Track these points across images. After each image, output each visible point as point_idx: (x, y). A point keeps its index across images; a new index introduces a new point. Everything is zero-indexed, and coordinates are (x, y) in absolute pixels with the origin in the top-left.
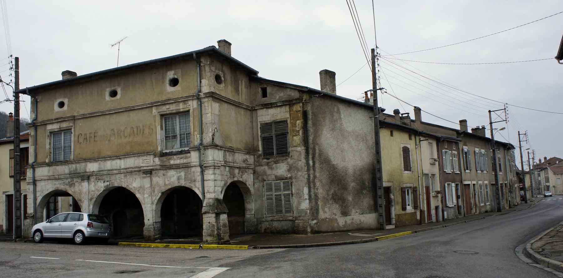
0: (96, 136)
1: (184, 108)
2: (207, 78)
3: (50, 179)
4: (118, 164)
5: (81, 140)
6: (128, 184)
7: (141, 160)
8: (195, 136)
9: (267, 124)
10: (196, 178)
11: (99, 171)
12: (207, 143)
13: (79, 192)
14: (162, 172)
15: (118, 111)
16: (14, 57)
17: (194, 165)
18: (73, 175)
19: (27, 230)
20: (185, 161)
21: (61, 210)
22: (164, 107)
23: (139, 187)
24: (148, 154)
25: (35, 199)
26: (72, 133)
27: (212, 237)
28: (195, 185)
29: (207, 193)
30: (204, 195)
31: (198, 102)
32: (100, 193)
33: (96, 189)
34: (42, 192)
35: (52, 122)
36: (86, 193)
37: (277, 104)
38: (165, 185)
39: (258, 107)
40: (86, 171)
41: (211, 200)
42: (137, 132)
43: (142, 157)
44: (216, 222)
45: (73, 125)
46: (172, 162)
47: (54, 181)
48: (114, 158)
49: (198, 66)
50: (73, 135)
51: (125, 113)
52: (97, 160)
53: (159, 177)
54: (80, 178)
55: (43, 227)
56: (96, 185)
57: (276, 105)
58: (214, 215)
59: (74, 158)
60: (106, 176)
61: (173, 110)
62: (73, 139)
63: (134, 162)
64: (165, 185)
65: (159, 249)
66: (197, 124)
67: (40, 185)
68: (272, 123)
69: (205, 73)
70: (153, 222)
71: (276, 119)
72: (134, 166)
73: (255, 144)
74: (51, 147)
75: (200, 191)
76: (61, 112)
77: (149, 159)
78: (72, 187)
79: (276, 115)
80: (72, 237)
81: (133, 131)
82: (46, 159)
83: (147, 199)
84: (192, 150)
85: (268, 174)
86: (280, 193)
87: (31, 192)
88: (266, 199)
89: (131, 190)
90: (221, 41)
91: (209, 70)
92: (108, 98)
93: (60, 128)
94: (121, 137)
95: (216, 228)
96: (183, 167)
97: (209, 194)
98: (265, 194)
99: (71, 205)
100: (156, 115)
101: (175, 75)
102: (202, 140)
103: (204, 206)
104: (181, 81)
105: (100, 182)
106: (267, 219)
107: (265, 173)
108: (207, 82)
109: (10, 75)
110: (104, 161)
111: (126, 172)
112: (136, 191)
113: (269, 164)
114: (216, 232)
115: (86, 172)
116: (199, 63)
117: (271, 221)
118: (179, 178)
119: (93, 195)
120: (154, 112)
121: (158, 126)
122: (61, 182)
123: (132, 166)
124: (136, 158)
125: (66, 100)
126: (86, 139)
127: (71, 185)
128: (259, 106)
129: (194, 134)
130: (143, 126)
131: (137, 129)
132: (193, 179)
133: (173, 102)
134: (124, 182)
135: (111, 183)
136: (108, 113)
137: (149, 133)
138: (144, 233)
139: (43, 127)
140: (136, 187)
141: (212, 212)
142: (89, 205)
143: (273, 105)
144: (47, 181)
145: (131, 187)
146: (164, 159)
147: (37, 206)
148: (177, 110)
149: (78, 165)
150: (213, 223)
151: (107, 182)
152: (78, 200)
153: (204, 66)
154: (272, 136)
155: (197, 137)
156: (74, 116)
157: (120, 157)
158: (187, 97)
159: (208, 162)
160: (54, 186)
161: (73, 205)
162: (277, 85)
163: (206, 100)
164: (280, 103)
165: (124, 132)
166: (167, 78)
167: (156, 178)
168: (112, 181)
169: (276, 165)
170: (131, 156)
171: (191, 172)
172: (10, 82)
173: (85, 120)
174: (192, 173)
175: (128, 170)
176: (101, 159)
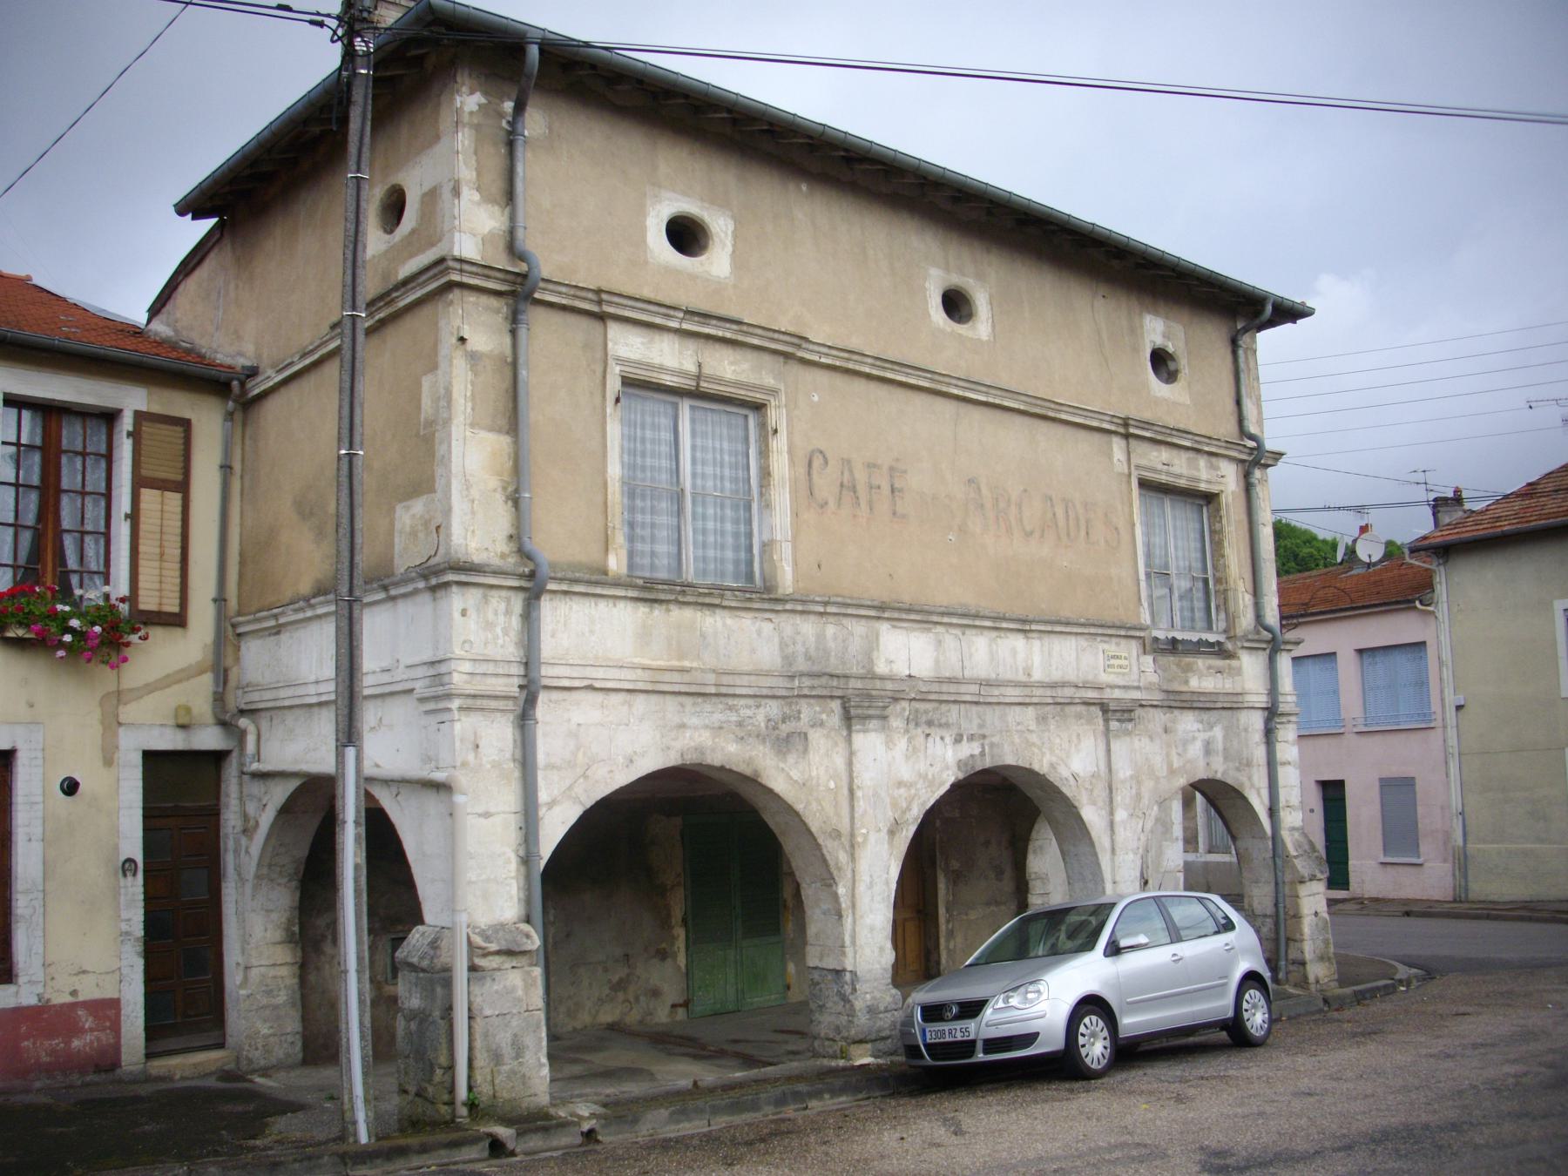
4: (1021, 656)
5: (825, 482)
6: (1054, 759)
13: (832, 785)
14: (1158, 718)
18: (807, 682)
19: (507, 1051)
21: (38, 904)
22: (1155, 454)
28: (1250, 778)
33: (920, 775)
34: (585, 776)
35: (658, 320)
36: (876, 794)
40: (874, 673)
43: (1101, 641)
45: (783, 389)
48: (1012, 626)
53: (1151, 738)
56: (921, 755)
61: (1180, 476)
62: (780, 464)
64: (1172, 772)
72: (1078, 676)
75: (1262, 802)
77: (1126, 658)
81: (1054, 514)
87: (496, 765)
93: (698, 377)
99: (128, 866)
104: (1187, 371)
105: (938, 739)
110: (957, 631)
111: (1050, 700)
112: (1084, 792)
119: (904, 805)
122: (718, 717)
127: (788, 742)
134: (1040, 749)
144: (621, 697)
145: (1064, 772)
149: (830, 630)
152: (824, 833)
165: (1019, 506)
171: (1238, 728)
173: (839, 380)
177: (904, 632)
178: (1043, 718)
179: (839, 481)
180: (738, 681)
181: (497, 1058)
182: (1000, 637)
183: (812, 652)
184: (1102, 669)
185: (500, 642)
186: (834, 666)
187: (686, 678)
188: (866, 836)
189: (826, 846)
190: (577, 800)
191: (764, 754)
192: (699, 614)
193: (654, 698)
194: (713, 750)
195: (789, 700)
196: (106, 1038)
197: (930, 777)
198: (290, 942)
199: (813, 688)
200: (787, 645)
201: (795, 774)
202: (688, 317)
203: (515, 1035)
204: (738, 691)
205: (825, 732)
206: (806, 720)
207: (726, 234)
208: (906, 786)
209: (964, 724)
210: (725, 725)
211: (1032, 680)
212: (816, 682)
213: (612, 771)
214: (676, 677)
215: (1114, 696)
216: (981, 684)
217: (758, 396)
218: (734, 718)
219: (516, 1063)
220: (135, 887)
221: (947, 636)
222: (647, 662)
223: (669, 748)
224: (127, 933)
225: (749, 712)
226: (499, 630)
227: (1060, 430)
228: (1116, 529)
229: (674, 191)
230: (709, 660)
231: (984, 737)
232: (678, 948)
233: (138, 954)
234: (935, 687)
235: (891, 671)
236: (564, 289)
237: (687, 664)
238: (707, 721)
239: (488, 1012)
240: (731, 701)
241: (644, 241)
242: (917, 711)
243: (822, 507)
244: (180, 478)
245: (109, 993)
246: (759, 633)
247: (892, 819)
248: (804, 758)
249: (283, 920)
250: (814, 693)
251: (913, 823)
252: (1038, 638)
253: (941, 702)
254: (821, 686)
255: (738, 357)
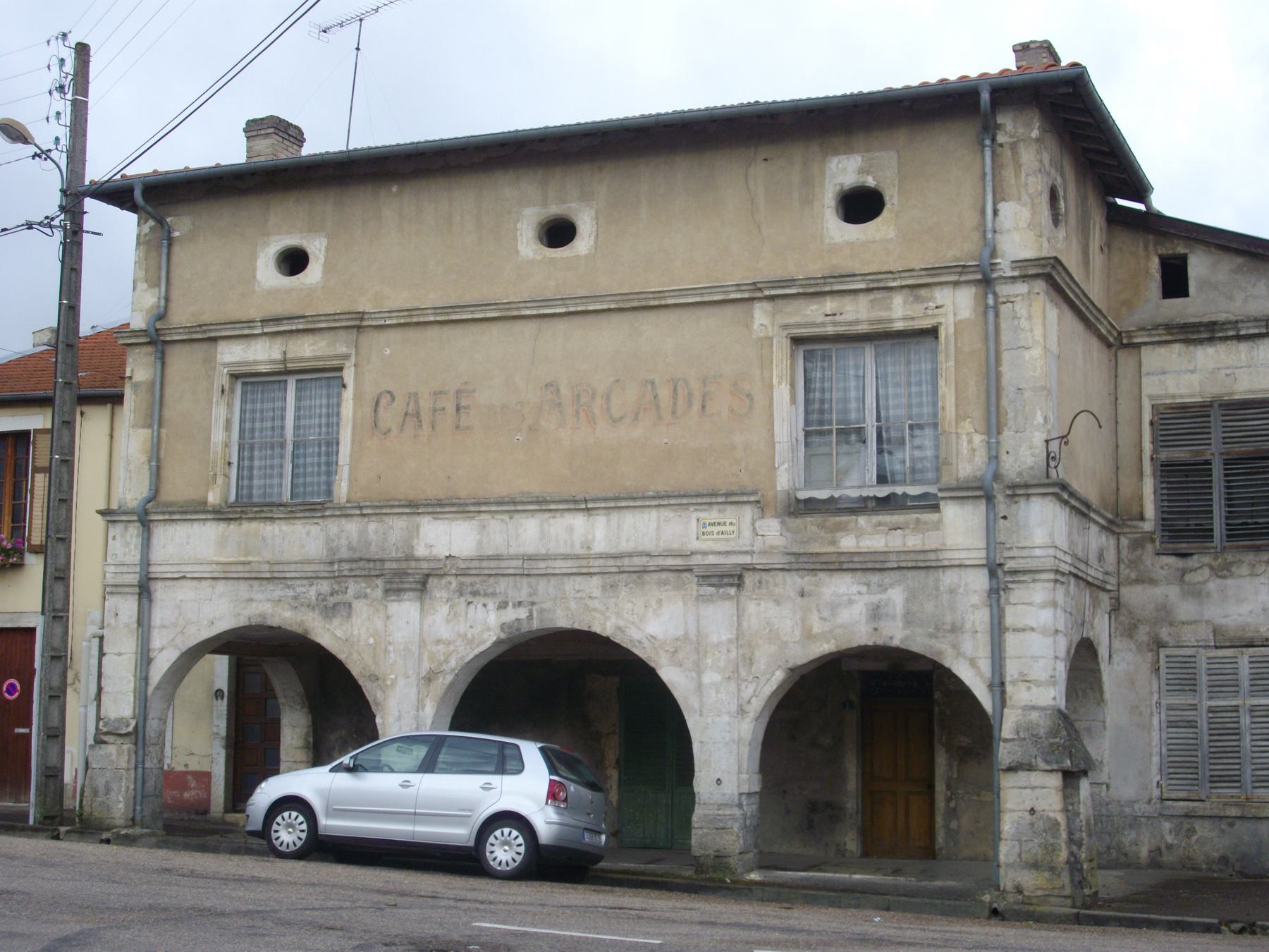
0: (467, 407)
1: (913, 319)
2: (1025, 197)
3: (225, 574)
5: (389, 416)
6: (621, 623)
7: (694, 522)
8: (964, 438)
9: (1182, 410)
10: (963, 618)
11: (481, 558)
12: (1020, 474)
13: (371, 641)
14: (793, 582)
15: (579, 309)
16: (72, 41)
17: (957, 562)
18: (346, 566)
19: (101, 790)
20: (913, 541)
22: (814, 307)
23: (677, 639)
24: (729, 500)
25: (145, 659)
26: (344, 386)
27: (1046, 874)
28: (955, 646)
29: (1014, 683)
30: (1003, 692)
31: (986, 298)
32: (476, 652)
34: (182, 632)
35: (246, 332)
37: (1238, 330)
38: (809, 636)
39: (1150, 335)
40: (413, 556)
41: (1034, 716)
42: (675, 404)
44: (1065, 810)
45: (354, 353)
46: (847, 543)
47: (243, 586)
48: (561, 507)
49: (988, 142)
50: (348, 395)
51: (616, 318)
52: (472, 508)
53: (777, 602)
54: (379, 582)
55: (323, 793)
57: (1231, 333)
58: (1055, 781)
59: (349, 493)
60: (511, 578)
61: (857, 322)
62: (347, 409)
63: (658, 527)
64: (809, 636)
65: (539, 902)
66: (973, 387)
67: (166, 601)
68: (1210, 406)
69: (1017, 176)
70: (741, 794)
71: (1224, 390)
73: (1127, 490)
74: (229, 437)
75: (979, 673)
76: (289, 291)
77: (731, 524)
78: (335, 617)
79: (1227, 375)
80: (471, 843)
81: (655, 397)
82: (207, 491)
83: (718, 692)
84: (952, 498)
85: (1183, 618)
86: (1234, 703)
87: (127, 625)
88: (1164, 725)
89: (635, 651)
90: (1032, 46)
91: (1036, 165)
92: (528, 246)
93: (285, 361)
94: (592, 420)
95: (1064, 835)
96: (903, 564)
97: (1029, 688)
98: (1163, 702)
99: (219, 694)
100: (771, 339)
101: (868, 173)
102: (994, 458)
103: (1006, 741)
104: (895, 200)
105: (480, 606)
106: (1168, 808)
107: (1164, 614)
108: (1025, 214)
109: (53, 114)
110: (506, 517)
112: (662, 654)
113: (1187, 578)
114: (1063, 855)
115: (410, 558)
116: (989, 129)
117: (1187, 816)
118: (876, 613)
119: (442, 658)
120: (762, 325)
121: (780, 383)
123: (648, 545)
124: (666, 513)
125: (317, 243)
126: (418, 415)
128: (1153, 332)
129: (960, 431)
130: (704, 381)
131: (675, 390)
132: (948, 619)
133: (862, 286)
134: (602, 613)
135: (535, 614)
136: (535, 312)
137: (732, 411)
138: (694, 841)
139: (200, 351)
140: (660, 636)
141: (1048, 768)
142: (420, 705)
143: (1222, 330)
144: (209, 582)
145: (635, 634)
146: (810, 523)
147: (151, 689)
148: (880, 321)
149: (373, 526)
150: (1052, 815)
151: (514, 606)
153: (1014, 147)
154: (1208, 463)
155: (970, 442)
156: (362, 315)
157: (590, 505)
158: (932, 271)
159: (1027, 551)
160: (244, 609)
161: (229, 692)
162: (1246, 248)
163: (1022, 288)
164: (1256, 327)
165: (608, 398)
166: (827, 186)
167: (762, 603)
168: (544, 606)
169: (1219, 581)
170: (647, 503)
171: (937, 589)
172: (53, 147)
173: (411, 333)
174: (946, 597)
175: (626, 561)
176: (494, 508)
177: (447, 522)
178: (612, 586)
179: (404, 411)
180: (286, 568)
181: (95, 792)
182: (554, 517)
183: (354, 544)
184: (695, 536)
185: (133, 553)
186: (374, 552)
187: (247, 568)
188: (394, 682)
189: (365, 686)
190: (176, 647)
191: (314, 619)
192: (262, 524)
193: (231, 582)
194: (272, 616)
195: (339, 580)
196: (202, 794)
197: (469, 636)
198: (307, 748)
199: (351, 570)
200: (333, 541)
201: (339, 633)
202: (264, 324)
203: (107, 782)
204: (288, 575)
205: (368, 602)
206: (352, 593)
207: (320, 250)
208: (444, 643)
209: (510, 593)
210: (283, 599)
211: (592, 552)
212: (354, 566)
213: (199, 630)
214: (240, 568)
215: (706, 562)
216: (524, 560)
217: (334, 362)
218: (291, 593)
219: (105, 797)
220: (222, 706)
221: (492, 522)
222: (223, 559)
223: (239, 615)
224: (217, 734)
225: (304, 590)
226: (132, 547)
227: (671, 316)
228: (748, 395)
229: (280, 234)
230: (267, 555)
231: (533, 604)
232: (611, 786)
233: (223, 747)
234: (476, 564)
235: (431, 553)
236: (181, 331)
237: (250, 559)
238: (269, 596)
239: (94, 766)
240: (289, 582)
241: (254, 277)
242: (462, 584)
243: (385, 434)
244: (36, 475)
245: (205, 768)
246: (308, 534)
247: (428, 669)
248: (348, 621)
249: (303, 733)
250: (353, 574)
251: (450, 673)
252: (605, 515)
253: (490, 575)
254: (359, 568)
255: (317, 339)
